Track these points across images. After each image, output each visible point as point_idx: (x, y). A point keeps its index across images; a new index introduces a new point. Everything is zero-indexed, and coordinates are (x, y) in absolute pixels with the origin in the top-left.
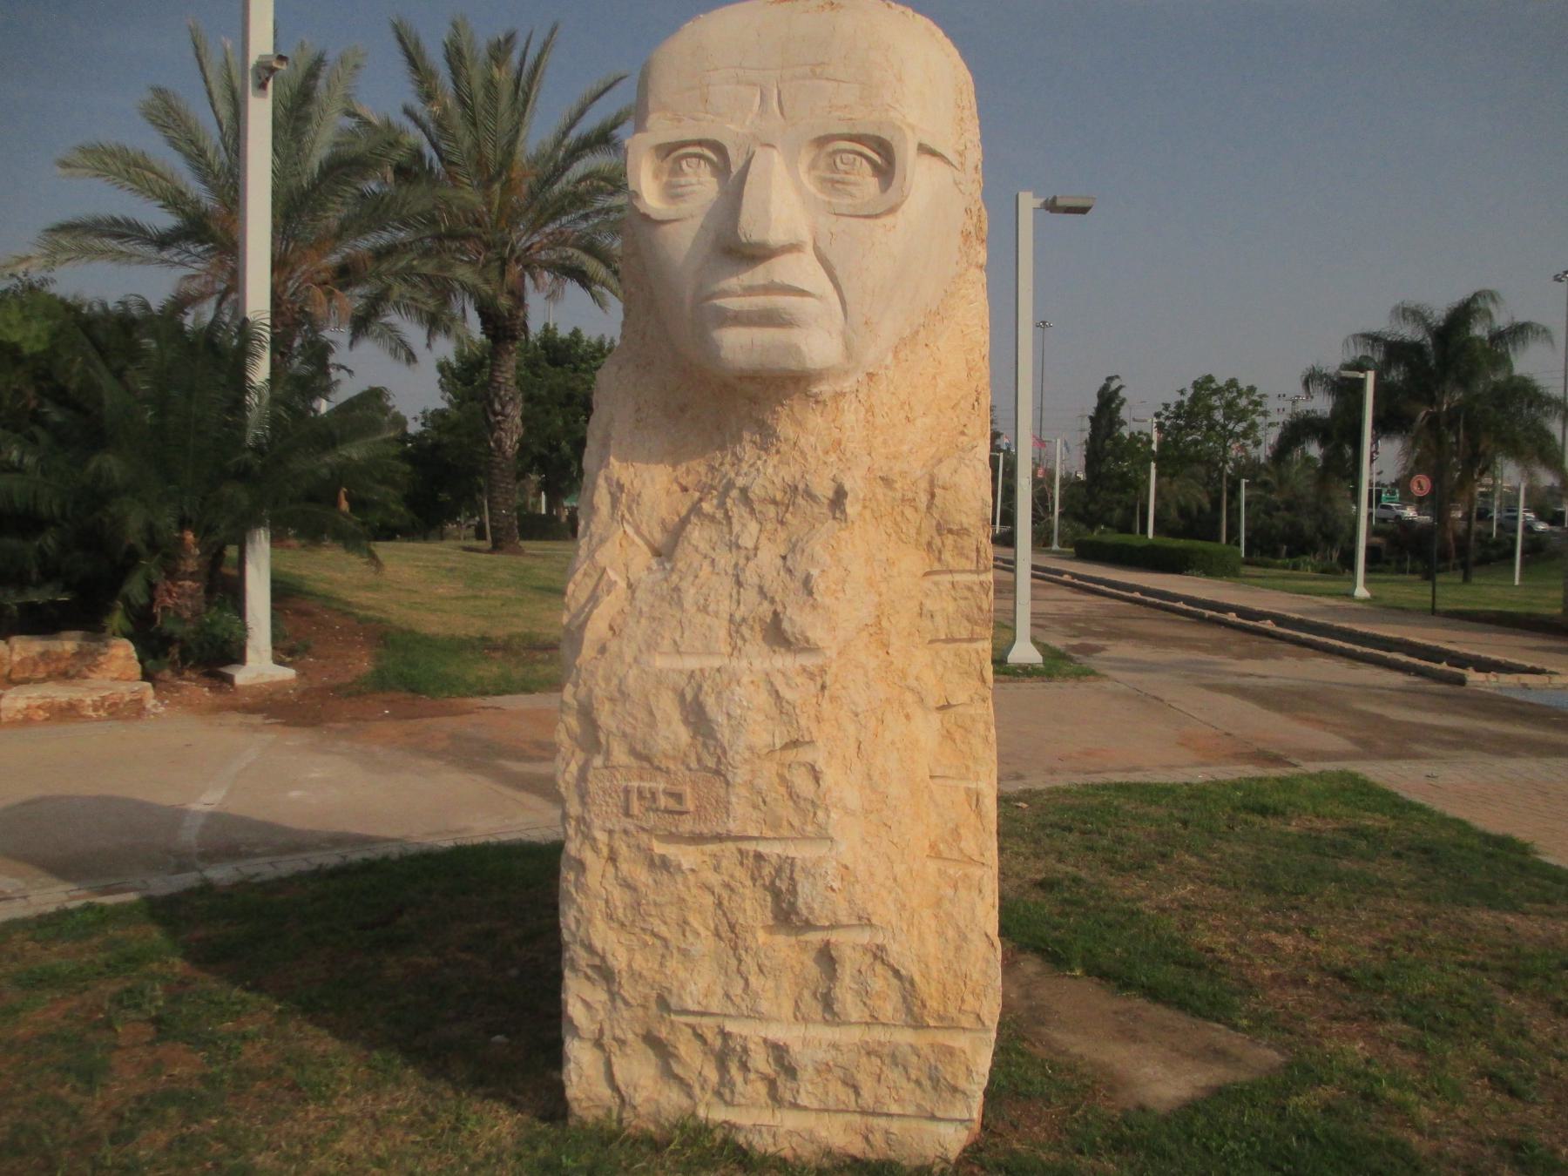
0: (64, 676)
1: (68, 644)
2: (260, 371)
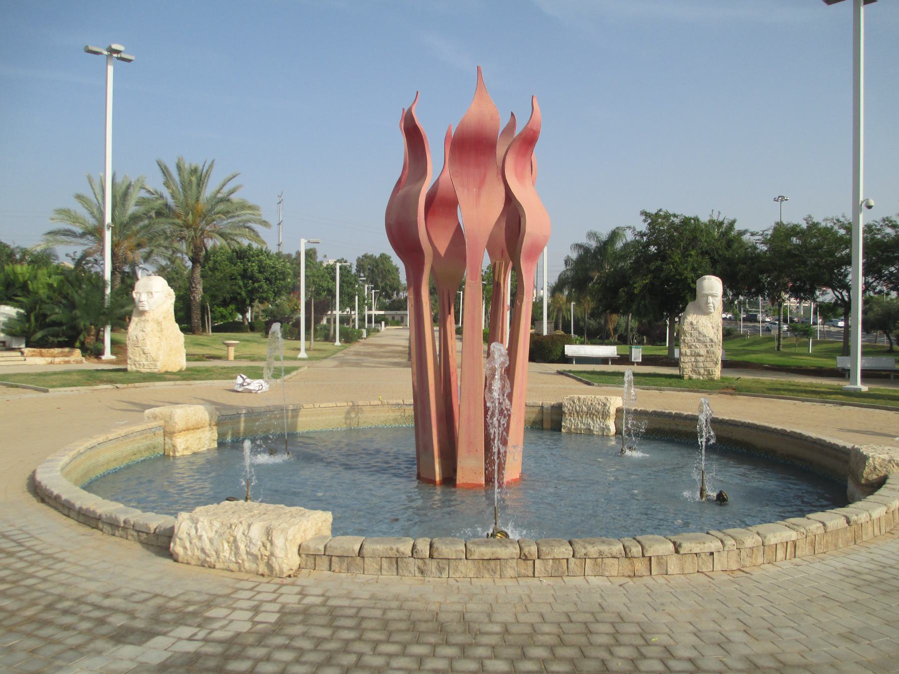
0: (66, 356)
1: (67, 350)
2: (108, 291)
